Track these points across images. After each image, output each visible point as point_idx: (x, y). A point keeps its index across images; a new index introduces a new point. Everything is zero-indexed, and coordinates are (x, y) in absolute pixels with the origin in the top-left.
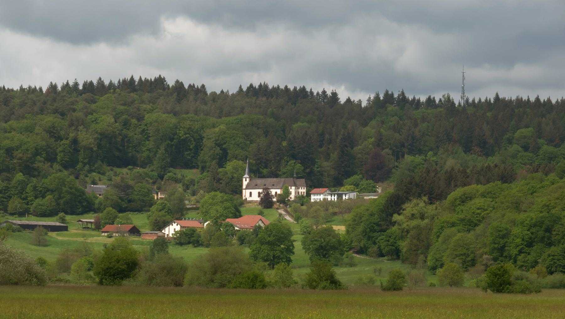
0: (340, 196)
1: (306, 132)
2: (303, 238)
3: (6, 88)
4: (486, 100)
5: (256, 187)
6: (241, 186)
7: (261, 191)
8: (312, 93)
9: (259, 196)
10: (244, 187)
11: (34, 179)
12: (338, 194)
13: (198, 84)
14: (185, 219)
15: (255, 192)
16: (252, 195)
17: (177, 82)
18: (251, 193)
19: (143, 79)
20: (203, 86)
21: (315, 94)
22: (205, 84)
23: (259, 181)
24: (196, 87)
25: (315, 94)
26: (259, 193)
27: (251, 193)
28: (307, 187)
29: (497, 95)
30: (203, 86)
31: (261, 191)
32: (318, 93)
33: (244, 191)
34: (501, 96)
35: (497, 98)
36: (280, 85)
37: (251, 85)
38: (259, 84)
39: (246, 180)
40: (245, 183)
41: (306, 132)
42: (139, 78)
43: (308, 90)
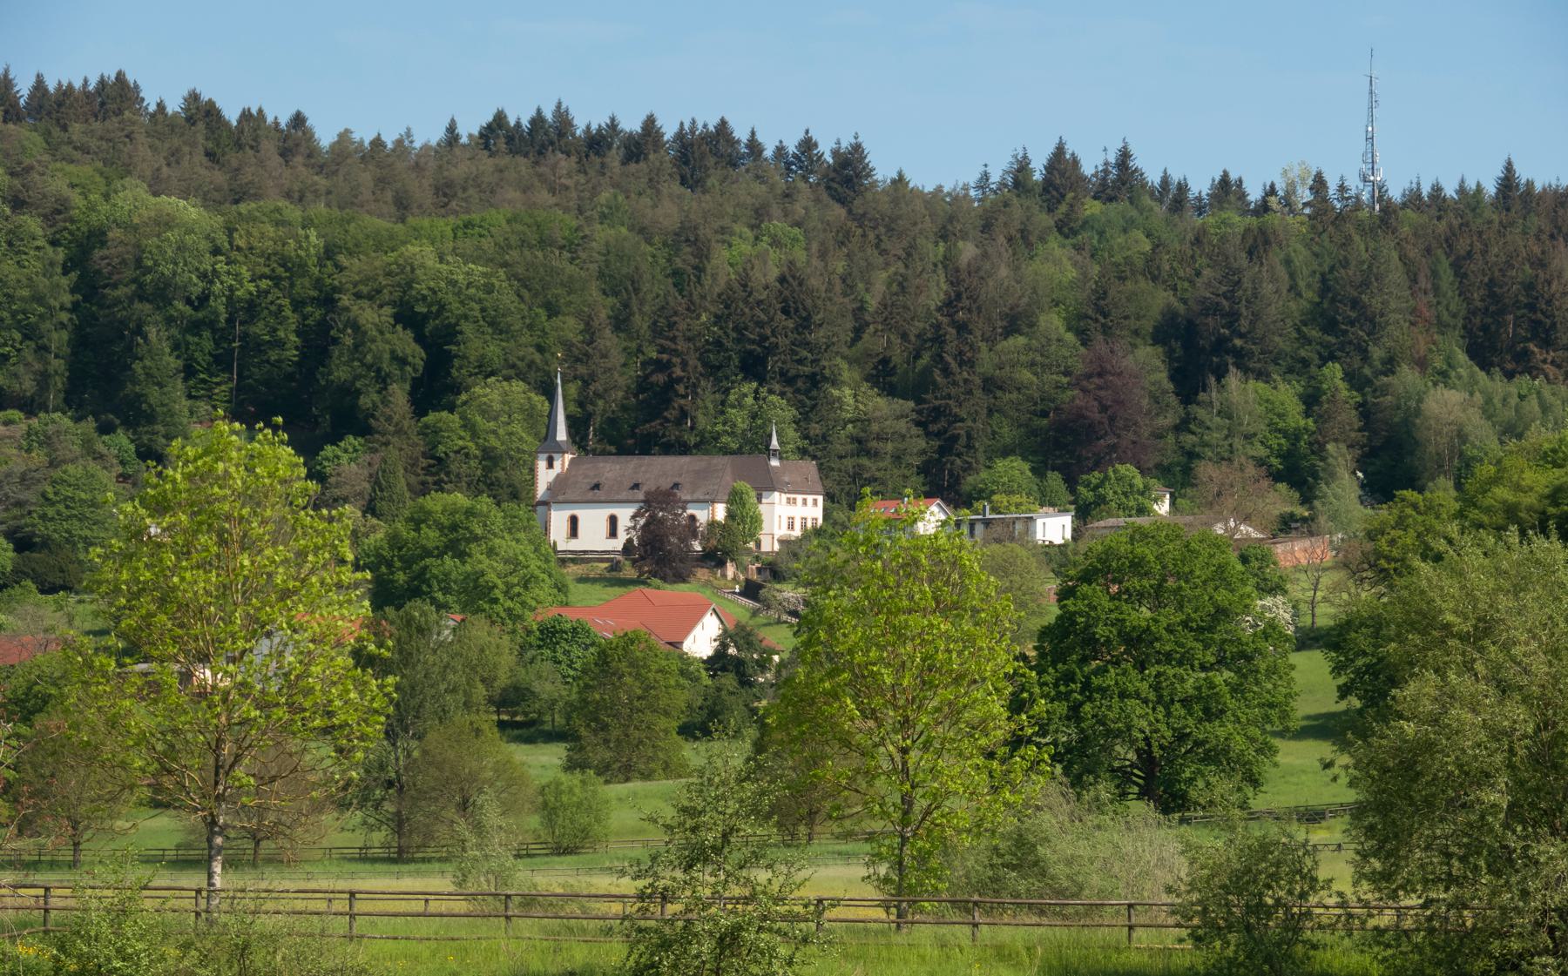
3: (325, 137)
4: (1462, 190)
5: (596, 493)
8: (754, 147)
13: (279, 113)
15: (593, 520)
17: (194, 97)
18: (574, 521)
19: (51, 86)
20: (298, 120)
21: (768, 153)
22: (306, 112)
23: (613, 469)
24: (270, 119)
25: (768, 153)
27: (574, 521)
28: (830, 497)
29: (1509, 168)
30: (298, 120)
32: (780, 150)
34: (1523, 173)
35: (1508, 181)
36: (1134, 149)
37: (500, 118)
38: (533, 113)
40: (545, 476)
42: (32, 81)
43: (741, 134)
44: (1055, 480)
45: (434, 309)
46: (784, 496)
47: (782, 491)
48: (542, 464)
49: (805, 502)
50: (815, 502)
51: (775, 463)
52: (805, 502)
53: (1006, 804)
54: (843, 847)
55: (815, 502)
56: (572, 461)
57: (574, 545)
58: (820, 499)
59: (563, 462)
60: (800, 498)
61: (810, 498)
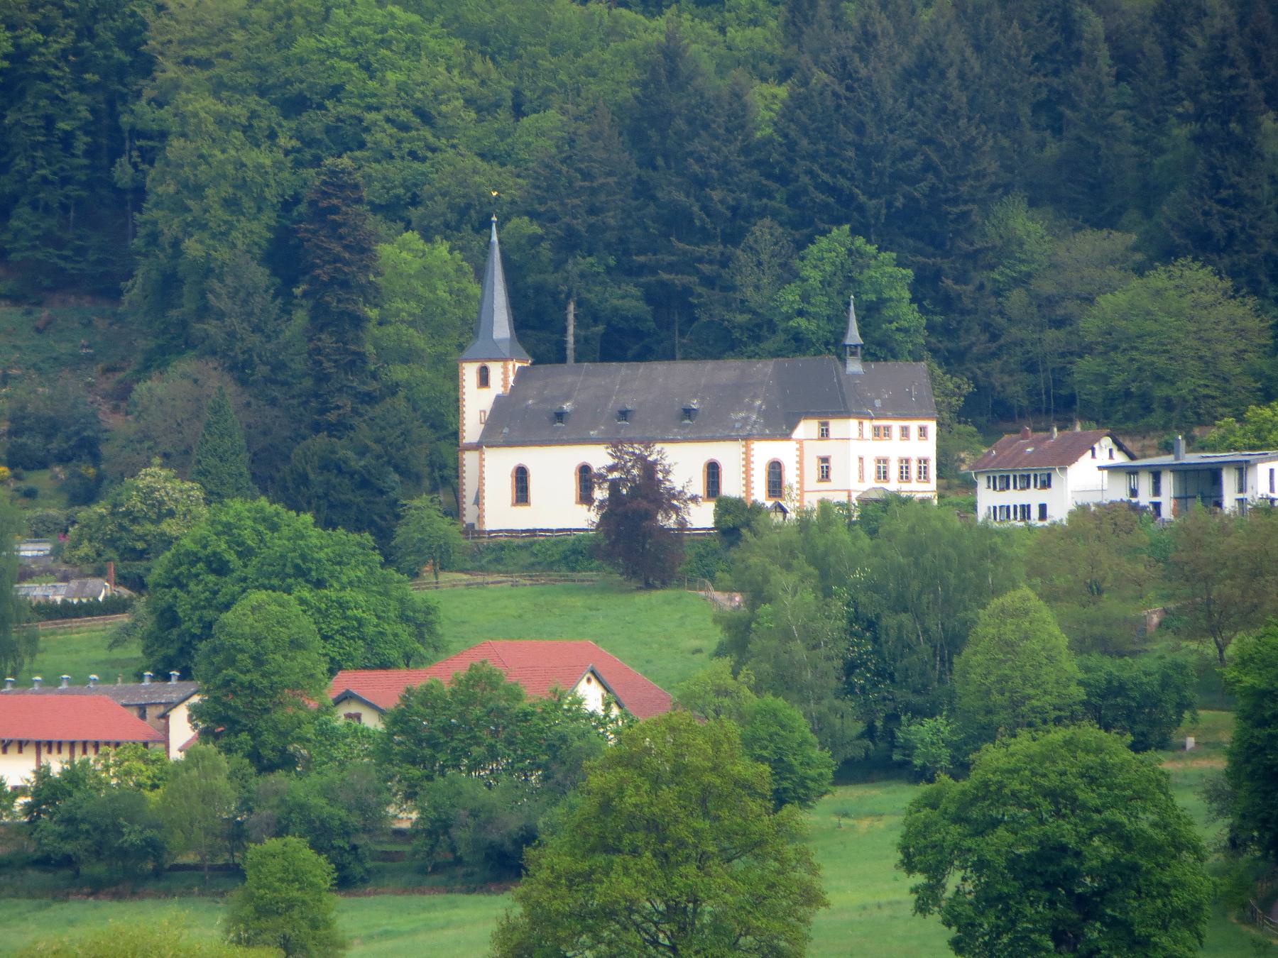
0: (1201, 484)
1: (529, 837)
2: (918, 805)
5: (554, 426)
6: (444, 420)
7: (599, 457)
9: (585, 497)
10: (472, 428)
11: (233, 233)
12: (1183, 472)
14: (52, 681)
16: (536, 488)
18: (521, 476)
23: (582, 383)
26: (586, 477)
27: (521, 476)
31: (599, 457)
33: (469, 459)
39: (484, 380)
40: (476, 403)
41: (529, 837)
44: (428, 826)
45: (279, 27)
46: (868, 425)
47: (861, 416)
48: (470, 372)
49: (905, 432)
50: (923, 432)
51: (855, 366)
52: (905, 432)
53: (302, 601)
54: (479, 579)
55: (923, 432)
56: (521, 374)
57: (522, 519)
58: (932, 426)
59: (502, 375)
60: (896, 425)
61: (914, 425)
